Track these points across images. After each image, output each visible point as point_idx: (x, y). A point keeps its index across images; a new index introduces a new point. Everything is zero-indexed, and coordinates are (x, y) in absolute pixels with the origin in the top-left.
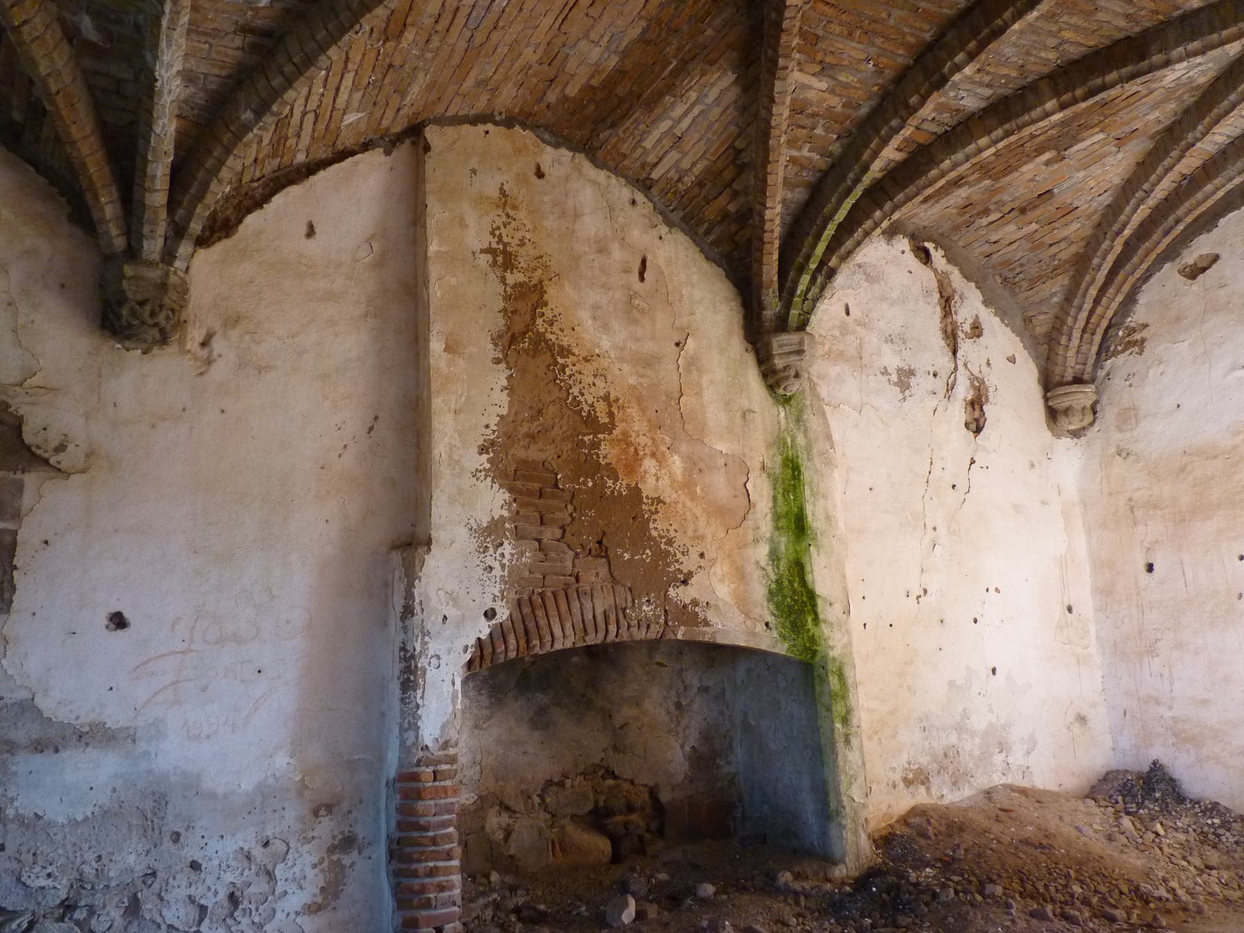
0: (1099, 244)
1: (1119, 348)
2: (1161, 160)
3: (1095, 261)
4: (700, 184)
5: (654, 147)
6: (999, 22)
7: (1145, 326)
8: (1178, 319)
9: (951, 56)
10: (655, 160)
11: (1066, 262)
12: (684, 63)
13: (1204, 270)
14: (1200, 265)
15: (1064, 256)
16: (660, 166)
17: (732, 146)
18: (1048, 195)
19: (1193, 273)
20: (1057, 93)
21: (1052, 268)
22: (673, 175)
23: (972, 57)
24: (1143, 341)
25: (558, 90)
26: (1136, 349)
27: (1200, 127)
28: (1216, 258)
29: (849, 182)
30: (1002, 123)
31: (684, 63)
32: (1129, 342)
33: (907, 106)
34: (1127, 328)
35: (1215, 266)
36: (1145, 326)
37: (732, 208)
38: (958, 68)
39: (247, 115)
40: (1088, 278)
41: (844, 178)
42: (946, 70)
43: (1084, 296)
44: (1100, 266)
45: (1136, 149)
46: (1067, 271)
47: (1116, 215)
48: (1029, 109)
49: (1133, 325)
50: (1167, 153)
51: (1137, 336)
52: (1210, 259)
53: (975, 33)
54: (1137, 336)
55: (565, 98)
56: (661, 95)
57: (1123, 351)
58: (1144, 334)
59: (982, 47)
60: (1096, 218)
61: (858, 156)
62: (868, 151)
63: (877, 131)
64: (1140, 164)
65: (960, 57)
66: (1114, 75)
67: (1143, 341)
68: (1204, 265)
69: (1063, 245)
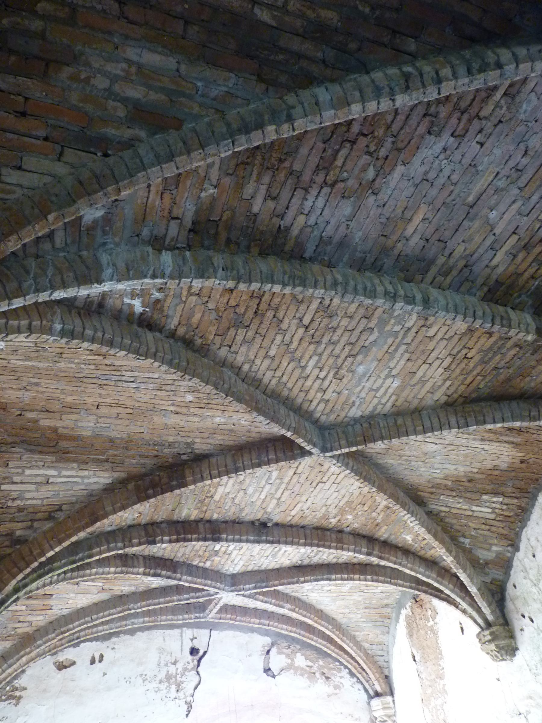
0: (47, 634)
1: (3, 698)
2: (110, 608)
3: (39, 642)
4: (20, 510)
5: (29, 476)
6: (190, 536)
7: (25, 689)
8: (45, 691)
9: (163, 535)
10: (18, 481)
11: (18, 634)
12: (107, 461)
13: (66, 667)
14: (64, 664)
15: (19, 631)
16: (15, 485)
17: (61, 506)
18: (49, 596)
19: (61, 667)
20: (145, 567)
21: (8, 634)
22: (14, 495)
23: (170, 542)
24: (20, 698)
25: (40, 416)
26: (14, 702)
27: (139, 604)
28: (74, 663)
29: (77, 558)
30: (123, 566)
31: (107, 461)
32: (11, 696)
33: (130, 541)
34: (13, 686)
35: (72, 667)
36: (25, 689)
37: (18, 533)
38: (162, 542)
39: (58, 327)
40: (28, 650)
41: (77, 554)
42: (157, 539)
43: (18, 660)
44: (39, 646)
45: (104, 596)
46: (14, 640)
47: (66, 624)
48: (134, 567)
49: (17, 685)
50: (115, 607)
51: (17, 694)
52: (70, 663)
53: (178, 534)
54: (17, 694)
55: (37, 421)
56: (75, 461)
57: (5, 700)
58: (23, 693)
59: (177, 541)
60: (52, 618)
61: (90, 548)
62: (98, 549)
63: (108, 543)
64: (96, 604)
65: (166, 538)
66: (164, 573)
67: (20, 698)
68: (67, 665)
69: (26, 625)
